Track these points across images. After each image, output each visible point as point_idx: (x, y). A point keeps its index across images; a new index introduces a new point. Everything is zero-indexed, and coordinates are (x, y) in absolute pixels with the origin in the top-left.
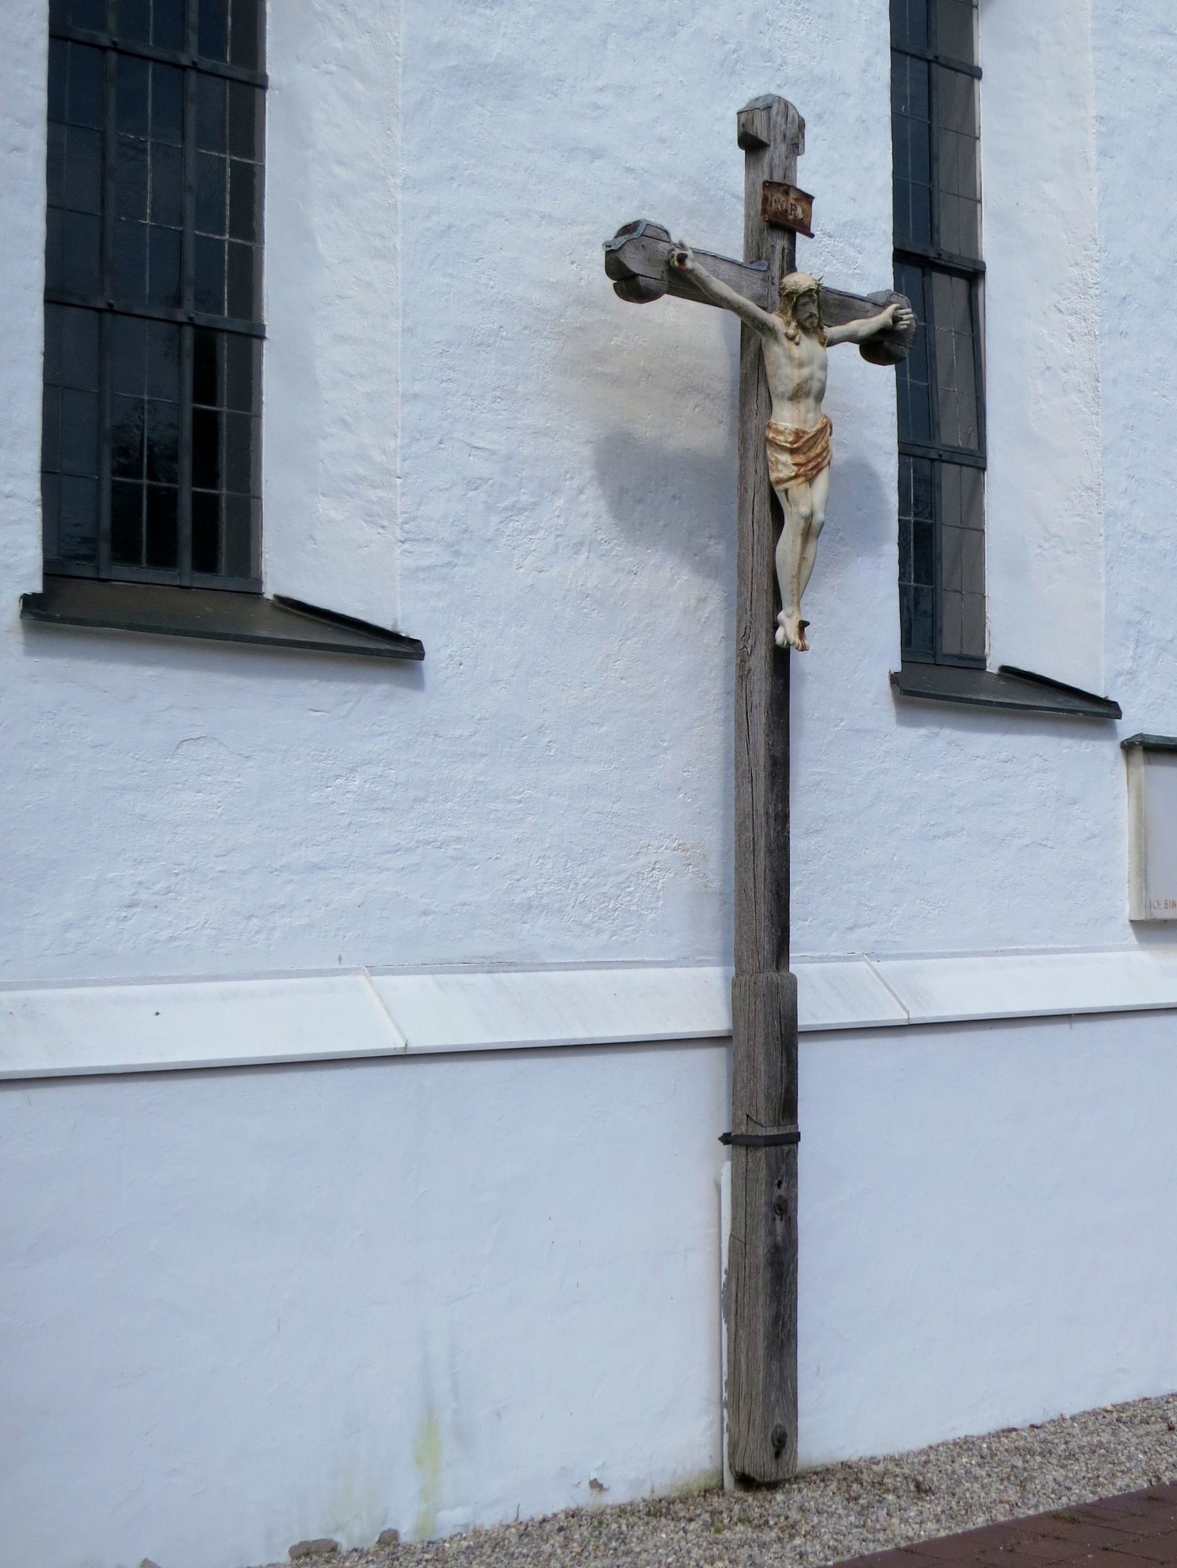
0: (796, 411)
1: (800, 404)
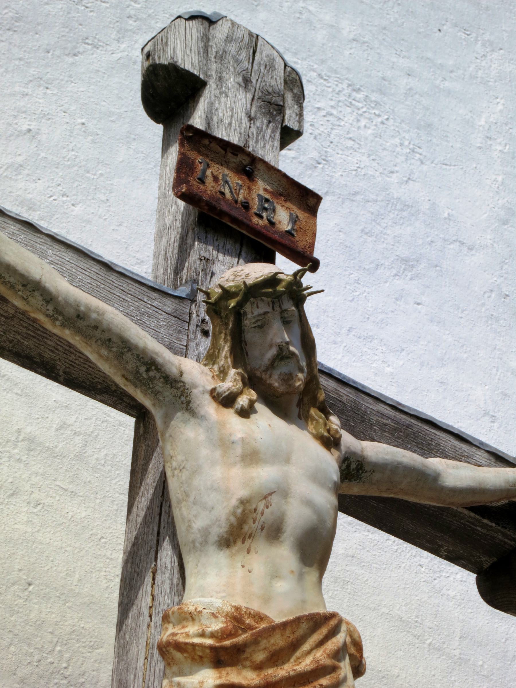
0: (240, 572)
1: (253, 556)
